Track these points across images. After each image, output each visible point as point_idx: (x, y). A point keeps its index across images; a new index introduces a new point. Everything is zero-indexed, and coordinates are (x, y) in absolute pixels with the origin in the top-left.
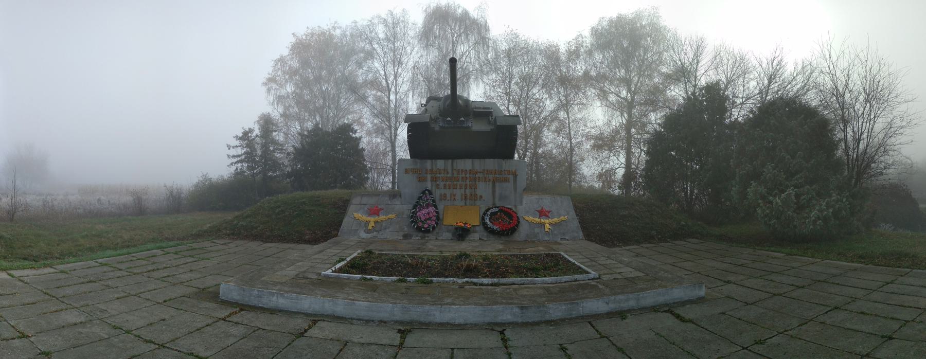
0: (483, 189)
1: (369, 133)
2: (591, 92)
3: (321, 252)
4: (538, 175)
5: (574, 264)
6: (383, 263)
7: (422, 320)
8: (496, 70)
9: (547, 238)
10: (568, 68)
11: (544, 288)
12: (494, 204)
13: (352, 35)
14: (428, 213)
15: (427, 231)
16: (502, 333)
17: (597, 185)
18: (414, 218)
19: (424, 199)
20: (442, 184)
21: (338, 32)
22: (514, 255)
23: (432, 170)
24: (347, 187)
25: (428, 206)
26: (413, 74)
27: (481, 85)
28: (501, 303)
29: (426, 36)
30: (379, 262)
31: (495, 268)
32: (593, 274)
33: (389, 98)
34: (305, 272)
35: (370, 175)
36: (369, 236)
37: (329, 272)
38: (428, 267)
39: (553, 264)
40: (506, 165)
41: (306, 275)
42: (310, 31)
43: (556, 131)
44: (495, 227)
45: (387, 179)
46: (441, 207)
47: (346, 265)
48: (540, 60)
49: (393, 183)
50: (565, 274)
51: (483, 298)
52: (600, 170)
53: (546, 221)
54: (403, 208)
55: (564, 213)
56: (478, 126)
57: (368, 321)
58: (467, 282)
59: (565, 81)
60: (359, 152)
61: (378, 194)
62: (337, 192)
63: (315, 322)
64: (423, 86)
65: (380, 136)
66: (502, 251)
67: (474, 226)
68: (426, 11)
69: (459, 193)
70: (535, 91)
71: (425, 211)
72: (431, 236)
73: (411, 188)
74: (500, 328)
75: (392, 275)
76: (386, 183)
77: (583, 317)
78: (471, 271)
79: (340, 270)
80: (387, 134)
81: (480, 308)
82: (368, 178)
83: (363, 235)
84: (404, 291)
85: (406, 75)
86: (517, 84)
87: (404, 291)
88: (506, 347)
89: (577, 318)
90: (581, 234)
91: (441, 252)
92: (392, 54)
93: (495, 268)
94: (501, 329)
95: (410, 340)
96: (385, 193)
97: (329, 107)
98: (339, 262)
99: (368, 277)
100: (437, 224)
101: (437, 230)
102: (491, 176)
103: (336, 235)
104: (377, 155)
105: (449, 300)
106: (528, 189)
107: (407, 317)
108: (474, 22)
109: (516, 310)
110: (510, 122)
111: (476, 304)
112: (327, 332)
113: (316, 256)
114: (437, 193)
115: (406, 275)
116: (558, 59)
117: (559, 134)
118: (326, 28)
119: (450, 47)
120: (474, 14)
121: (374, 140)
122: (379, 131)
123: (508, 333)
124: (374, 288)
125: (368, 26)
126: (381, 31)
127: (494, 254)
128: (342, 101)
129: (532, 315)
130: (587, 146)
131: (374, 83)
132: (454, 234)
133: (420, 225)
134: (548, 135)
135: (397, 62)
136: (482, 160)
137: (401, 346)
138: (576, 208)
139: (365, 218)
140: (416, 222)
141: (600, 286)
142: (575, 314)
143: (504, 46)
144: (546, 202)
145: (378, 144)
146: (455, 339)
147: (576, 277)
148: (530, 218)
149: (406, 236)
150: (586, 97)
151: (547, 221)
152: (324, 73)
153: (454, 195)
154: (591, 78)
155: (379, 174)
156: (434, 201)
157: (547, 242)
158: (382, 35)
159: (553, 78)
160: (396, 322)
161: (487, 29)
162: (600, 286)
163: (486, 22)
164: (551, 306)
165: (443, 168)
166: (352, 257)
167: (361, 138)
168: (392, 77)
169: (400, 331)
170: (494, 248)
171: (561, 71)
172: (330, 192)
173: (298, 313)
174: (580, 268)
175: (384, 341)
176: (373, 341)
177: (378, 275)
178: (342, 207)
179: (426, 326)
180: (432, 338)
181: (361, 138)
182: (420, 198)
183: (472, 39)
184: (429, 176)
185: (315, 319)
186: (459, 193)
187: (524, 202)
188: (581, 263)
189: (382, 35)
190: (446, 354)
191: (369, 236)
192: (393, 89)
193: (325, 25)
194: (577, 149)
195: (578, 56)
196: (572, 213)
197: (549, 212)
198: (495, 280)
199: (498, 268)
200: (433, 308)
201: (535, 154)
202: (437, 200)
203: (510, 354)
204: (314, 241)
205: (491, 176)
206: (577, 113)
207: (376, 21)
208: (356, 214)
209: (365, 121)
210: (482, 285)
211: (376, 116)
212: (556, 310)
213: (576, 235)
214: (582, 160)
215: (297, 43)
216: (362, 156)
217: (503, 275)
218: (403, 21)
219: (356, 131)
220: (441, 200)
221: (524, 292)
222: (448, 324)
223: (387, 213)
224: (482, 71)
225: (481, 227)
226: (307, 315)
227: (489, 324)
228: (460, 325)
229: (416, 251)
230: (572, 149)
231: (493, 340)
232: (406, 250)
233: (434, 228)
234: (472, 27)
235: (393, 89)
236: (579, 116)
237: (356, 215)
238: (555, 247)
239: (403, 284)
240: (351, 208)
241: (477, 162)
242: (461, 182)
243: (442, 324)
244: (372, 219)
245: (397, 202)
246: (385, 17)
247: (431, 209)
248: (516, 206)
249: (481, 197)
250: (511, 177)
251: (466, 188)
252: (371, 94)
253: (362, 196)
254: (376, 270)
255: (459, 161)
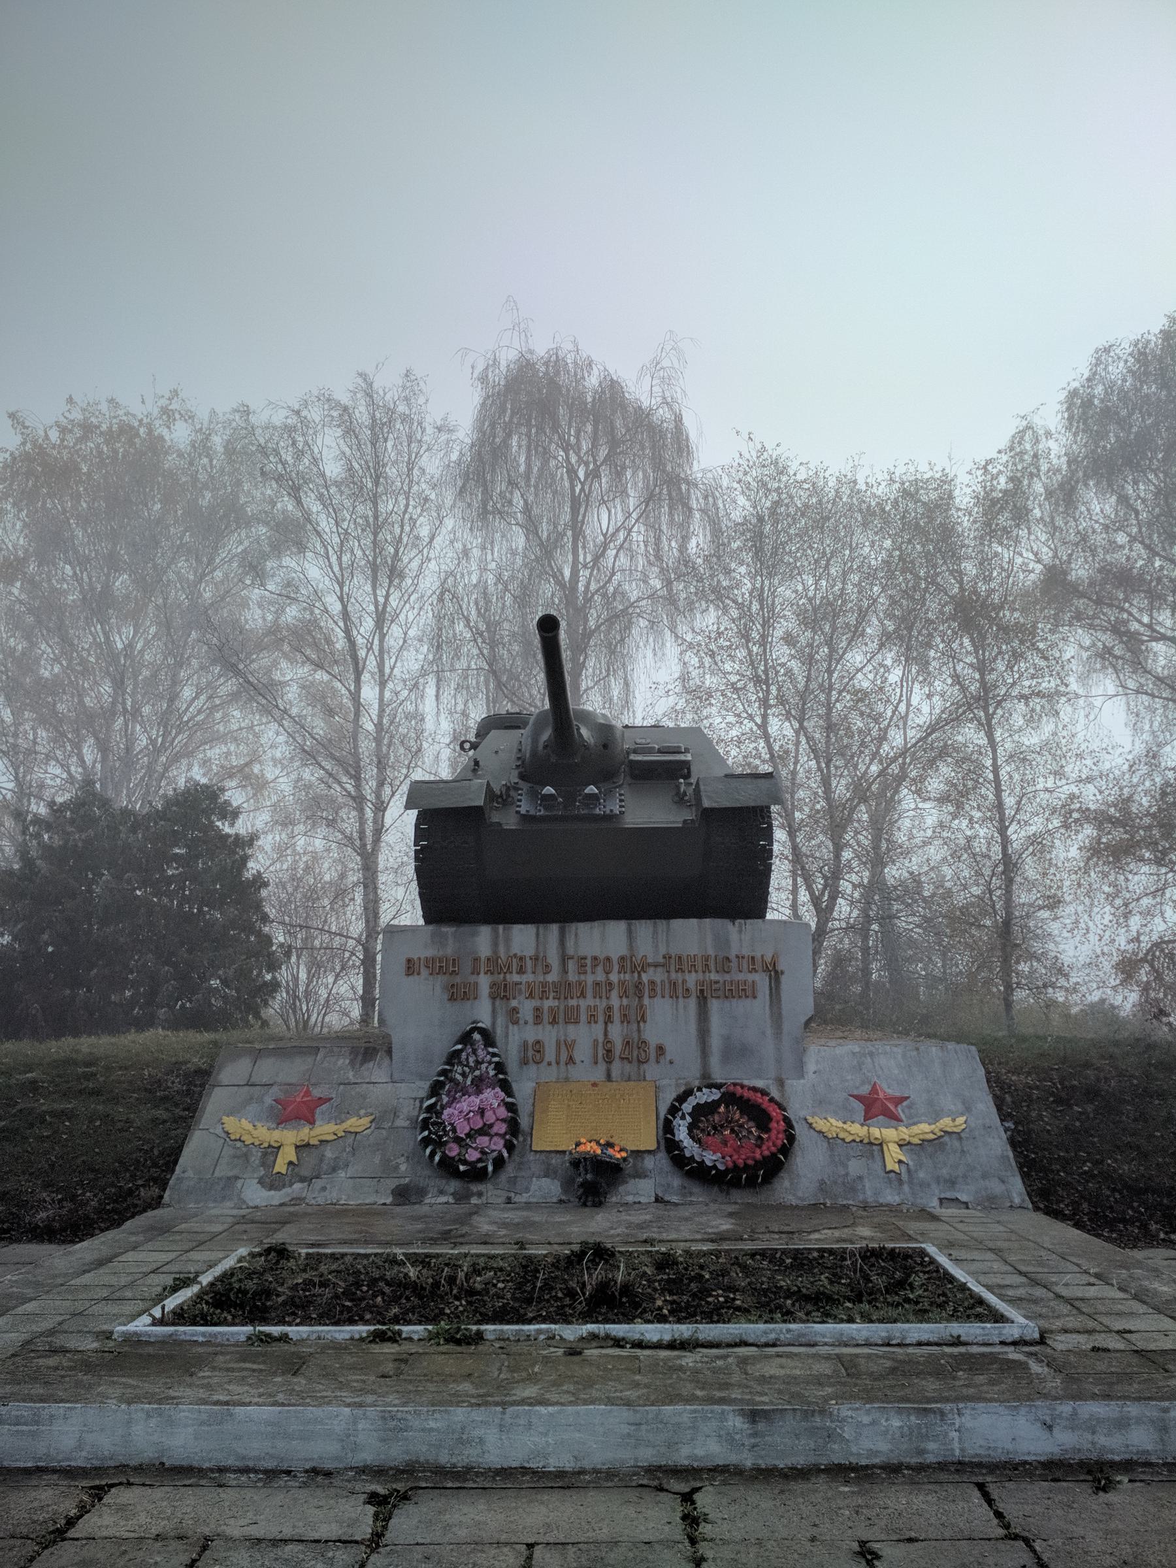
0: (668, 1023)
1: (285, 821)
2: (1075, 646)
3: (101, 1263)
4: (893, 964)
5: (963, 1287)
6: (323, 1284)
7: (444, 1459)
8: (719, 596)
9: (891, 1197)
10: (984, 563)
11: (839, 1357)
12: (705, 1075)
13: (230, 450)
14: (482, 1112)
15: (477, 1174)
16: (687, 1498)
17: (1127, 1001)
18: (431, 1127)
19: (469, 1059)
20: (527, 1008)
21: (180, 435)
22: (763, 1253)
23: (493, 961)
24: (197, 1020)
25: (479, 1085)
26: (439, 618)
27: (672, 649)
28: (690, 1400)
29: (483, 477)
30: (309, 1283)
31: (689, 1289)
32: (1020, 1324)
33: (356, 697)
34: (52, 1332)
35: (283, 975)
36: (276, 1197)
37: (141, 1325)
38: (471, 1292)
39: (893, 1279)
40: (740, 937)
41: (59, 1341)
42: (77, 415)
43: (943, 799)
44: (710, 1158)
45: (343, 988)
46: (523, 1088)
47: (199, 1297)
48: (873, 549)
49: (367, 1001)
50: (922, 1315)
51: (637, 1385)
52: (1122, 941)
53: (897, 1130)
54: (399, 1091)
55: (949, 1105)
56: (644, 811)
57: (271, 1474)
58: (594, 1336)
59: (973, 614)
60: (244, 893)
61: (308, 1044)
62: (157, 1043)
63: (98, 1493)
64: (471, 658)
65: (322, 831)
66: (735, 1243)
67: (638, 1154)
68: (483, 379)
69: (584, 1036)
70: (856, 657)
71: (469, 1103)
72: (491, 1192)
73: (423, 1024)
74: (679, 1483)
75: (351, 1322)
76: (339, 1000)
77: (962, 1467)
78: (613, 1302)
79: (180, 1316)
80: (349, 821)
81: (624, 1413)
82: (275, 986)
83: (256, 1195)
84: (389, 1368)
85: (414, 620)
86: (789, 640)
87: (389, 1368)
88: (693, 1541)
89: (942, 1466)
90: (1016, 1187)
91: (521, 1245)
92: (367, 541)
93: (689, 1289)
94: (684, 1488)
95: (405, 1524)
96: (340, 1039)
97: (136, 712)
98: (175, 1289)
99: (275, 1330)
100: (510, 1147)
101: (510, 1170)
102: (692, 979)
103: (157, 1203)
104: (312, 896)
105: (531, 1391)
106: (835, 1013)
107: (395, 1454)
108: (641, 419)
109: (736, 1422)
110: (745, 796)
111: (610, 1401)
112: (143, 1518)
113: (87, 1279)
114: (511, 1042)
115: (396, 1320)
116: (948, 532)
117: (959, 806)
118: (139, 410)
119: (566, 517)
120: (641, 391)
121: (301, 842)
122: (317, 810)
123: (705, 1500)
124: (295, 1364)
125: (290, 430)
126: (331, 454)
127: (695, 1247)
128: (187, 693)
129: (788, 1445)
130: (1069, 851)
131: (304, 640)
132: (567, 1185)
133: (453, 1151)
134: (919, 817)
135: (387, 570)
136: (662, 924)
137: (376, 1541)
138: (999, 1089)
139: (265, 1134)
140: (440, 1144)
141: (1035, 1367)
142: (933, 1451)
143: (740, 508)
144: (890, 1063)
145: (315, 857)
146: (539, 1515)
147: (957, 1328)
148: (831, 1124)
149: (403, 1195)
150: (1058, 668)
151: (890, 1134)
152: (121, 583)
153: (570, 1046)
154: (1074, 590)
155: (316, 968)
156: (500, 1068)
157: (894, 1210)
158: (333, 469)
159: (933, 605)
160: (362, 1470)
161: (682, 446)
162: (1035, 1367)
163: (678, 419)
164: (845, 1411)
165: (529, 951)
166: (218, 1271)
167: (252, 839)
168: (369, 623)
169: (373, 1499)
170: (700, 1225)
171: (959, 574)
172: (133, 1042)
173: (40, 1470)
174: (981, 1302)
175: (326, 1531)
176: (288, 1532)
177: (306, 1321)
178: (181, 1097)
179: (456, 1479)
180: (469, 1516)
181: (252, 839)
182: (453, 1058)
183: (635, 485)
184: (484, 982)
185: (98, 1481)
186: (584, 1036)
187: (811, 1066)
188: (989, 1288)
189: (333, 469)
190: (511, 1558)
191: (276, 1197)
192: (372, 663)
193: (137, 402)
194: (1030, 869)
195: (1021, 516)
196: (985, 1106)
197: (899, 1101)
198: (684, 1330)
199: (705, 1292)
200: (478, 1415)
201: (875, 888)
202: (512, 1066)
203: (698, 1561)
204: (71, 1230)
205: (692, 979)
206: (1020, 731)
207: (315, 414)
208: (232, 1121)
209: (270, 773)
210: (639, 1345)
211: (309, 756)
212: (871, 1431)
213: (997, 1188)
214: (1054, 903)
215: (27, 457)
216: (258, 906)
217: (714, 1315)
218: (406, 419)
219: (235, 814)
220: (524, 1062)
221: (771, 1369)
222: (524, 1470)
223: (340, 1115)
224: (671, 600)
225: (662, 1156)
226: (70, 1473)
227: (651, 1470)
228: (561, 1474)
229: (434, 1241)
230: (1009, 866)
231: (658, 1518)
232: (401, 1237)
233: (499, 1163)
234: (635, 441)
235: (372, 663)
236: (1031, 739)
237: (231, 1123)
238: (913, 1227)
239: (389, 1349)
240: (215, 1101)
241: (644, 929)
242: (590, 1001)
243: (505, 1473)
244: (289, 1137)
245: (377, 1072)
246: (345, 399)
247: (492, 1097)
248: (781, 1083)
249: (661, 1050)
250: (762, 981)
251: (609, 1020)
252: (292, 675)
253: (258, 1055)
254: (300, 1308)
255: (583, 928)
